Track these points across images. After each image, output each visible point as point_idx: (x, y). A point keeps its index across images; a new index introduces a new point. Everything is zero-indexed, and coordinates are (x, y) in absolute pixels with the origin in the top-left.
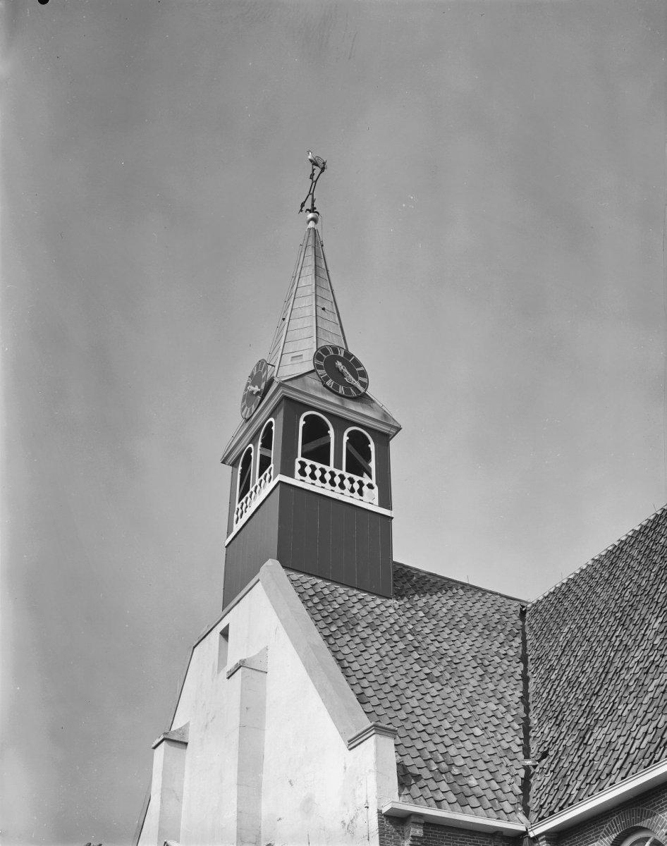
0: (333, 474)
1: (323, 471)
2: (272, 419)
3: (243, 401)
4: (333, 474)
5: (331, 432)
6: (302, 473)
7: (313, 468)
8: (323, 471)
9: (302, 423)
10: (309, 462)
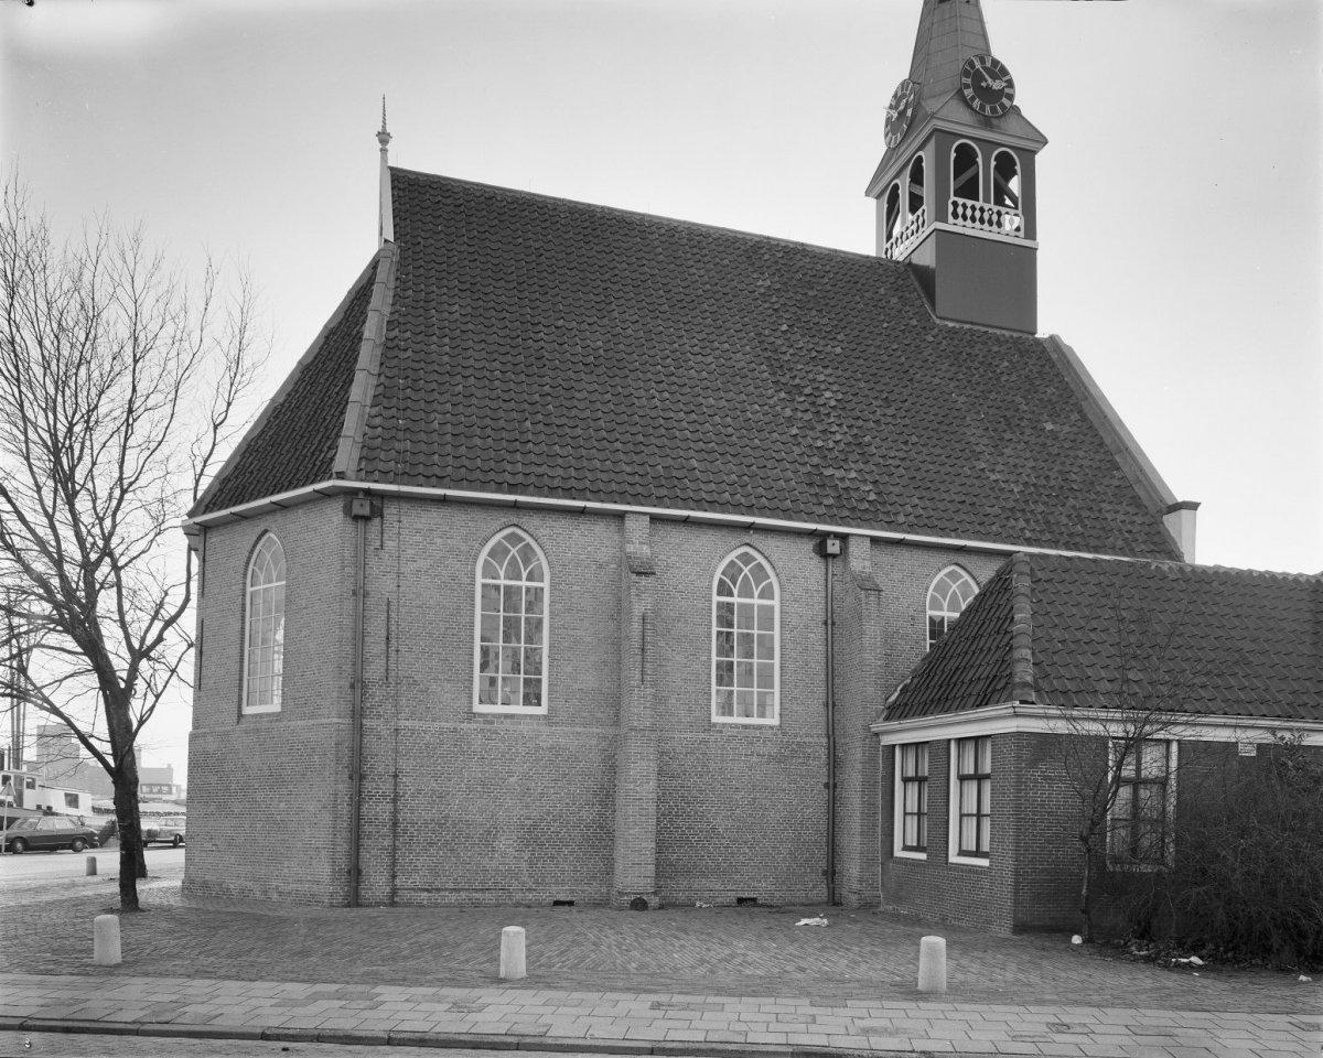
0: (982, 210)
1: (973, 208)
2: (920, 153)
3: (887, 126)
4: (982, 210)
5: (980, 160)
6: (955, 215)
7: (964, 206)
8: (973, 208)
9: (953, 155)
10: (961, 201)
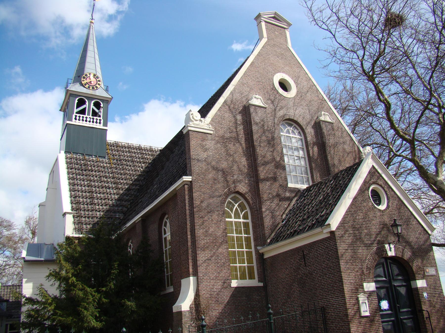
0: (86, 118)
7: (80, 117)
9: (76, 101)
